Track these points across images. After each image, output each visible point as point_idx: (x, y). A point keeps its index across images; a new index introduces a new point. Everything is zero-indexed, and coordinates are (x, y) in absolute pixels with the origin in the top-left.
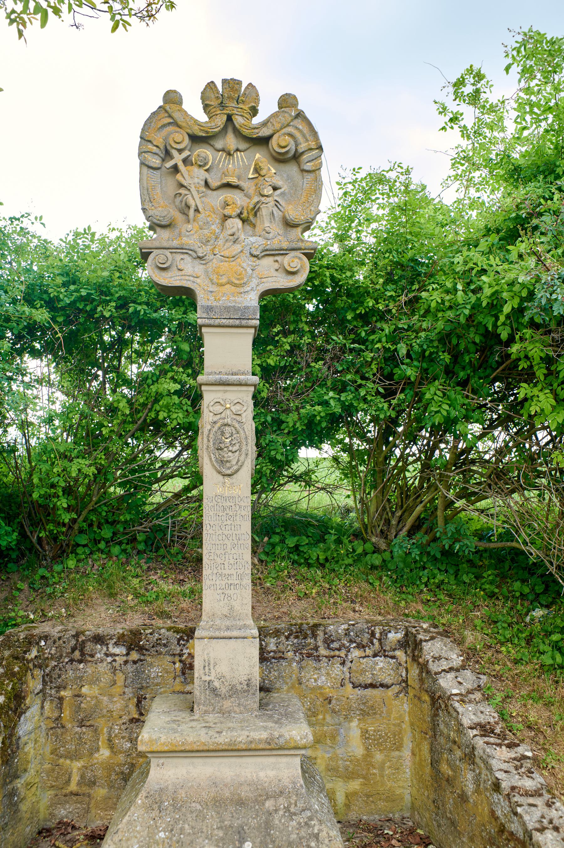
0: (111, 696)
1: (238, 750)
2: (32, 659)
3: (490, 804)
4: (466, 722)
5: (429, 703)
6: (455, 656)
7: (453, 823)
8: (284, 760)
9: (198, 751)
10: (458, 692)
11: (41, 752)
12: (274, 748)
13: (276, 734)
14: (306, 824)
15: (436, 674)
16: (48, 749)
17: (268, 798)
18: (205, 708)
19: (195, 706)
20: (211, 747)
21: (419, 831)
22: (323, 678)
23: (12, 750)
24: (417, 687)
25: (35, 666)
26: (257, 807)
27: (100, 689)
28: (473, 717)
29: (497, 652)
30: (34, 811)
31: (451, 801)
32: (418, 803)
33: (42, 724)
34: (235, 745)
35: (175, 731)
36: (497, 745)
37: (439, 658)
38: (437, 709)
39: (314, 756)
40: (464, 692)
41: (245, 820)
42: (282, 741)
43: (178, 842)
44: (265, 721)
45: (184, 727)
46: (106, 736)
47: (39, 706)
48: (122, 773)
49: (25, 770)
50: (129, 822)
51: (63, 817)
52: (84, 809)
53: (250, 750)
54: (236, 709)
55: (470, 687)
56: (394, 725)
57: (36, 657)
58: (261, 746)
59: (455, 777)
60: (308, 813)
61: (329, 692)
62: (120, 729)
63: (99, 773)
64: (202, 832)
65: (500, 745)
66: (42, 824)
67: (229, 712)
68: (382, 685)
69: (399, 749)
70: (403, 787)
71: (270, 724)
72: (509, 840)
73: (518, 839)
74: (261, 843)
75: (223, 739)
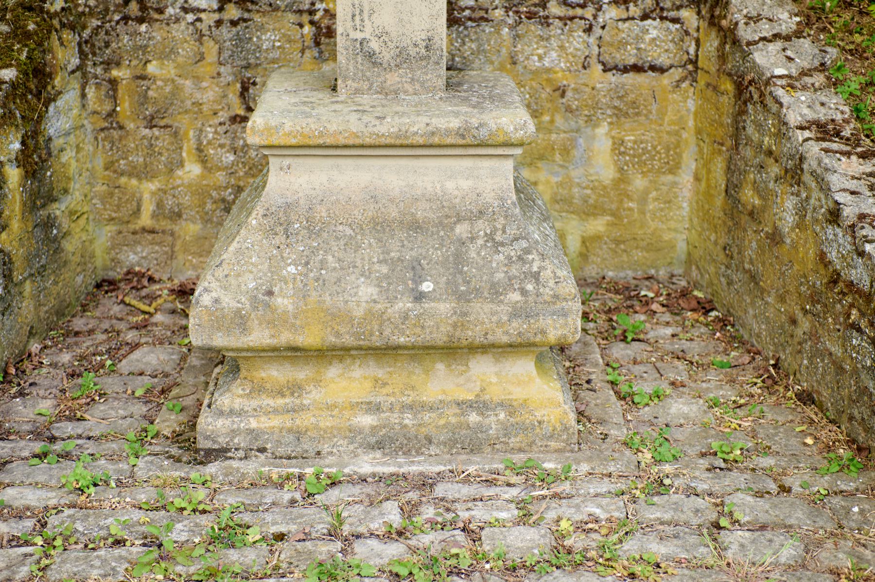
0: (197, 79)
1: (412, 146)
2: (56, 14)
3: (819, 243)
4: (793, 118)
5: (731, 95)
6: (785, 16)
7: (753, 278)
8: (486, 163)
9: (346, 146)
10: (785, 72)
11: (89, 166)
12: (472, 144)
13: (475, 122)
14: (520, 258)
15: (749, 44)
16: (99, 163)
17: (459, 221)
18: (355, 85)
19: (339, 82)
20: (368, 141)
21: (696, 293)
22: (554, 55)
23: (40, 157)
24: (713, 70)
25: (63, 25)
26: (442, 233)
27: (178, 66)
28: (806, 111)
29: (861, 13)
30: (87, 256)
31: (754, 244)
32: (697, 254)
33: (86, 122)
34: (406, 137)
35: (308, 116)
36: (843, 153)
37: (757, 19)
38: (745, 103)
39: (533, 179)
40: (794, 72)
41: (423, 251)
42: (483, 133)
43: (317, 280)
44: (456, 105)
45: (321, 110)
46: (193, 143)
47: (78, 92)
48: (223, 200)
49: (66, 191)
50: (238, 251)
51: (133, 265)
52: (166, 253)
53: (431, 146)
54: (408, 87)
55: (806, 65)
56: (668, 133)
57: (63, 9)
58: (449, 141)
59: (764, 209)
60: (524, 244)
61: (562, 79)
62: (216, 132)
63: (186, 200)
64: (355, 267)
65: (848, 154)
66: (101, 275)
67: (396, 92)
68: (653, 68)
69: (672, 171)
70: (676, 230)
71: (464, 109)
72: (844, 294)
73: (859, 292)
74: (447, 283)
75: (388, 128)
